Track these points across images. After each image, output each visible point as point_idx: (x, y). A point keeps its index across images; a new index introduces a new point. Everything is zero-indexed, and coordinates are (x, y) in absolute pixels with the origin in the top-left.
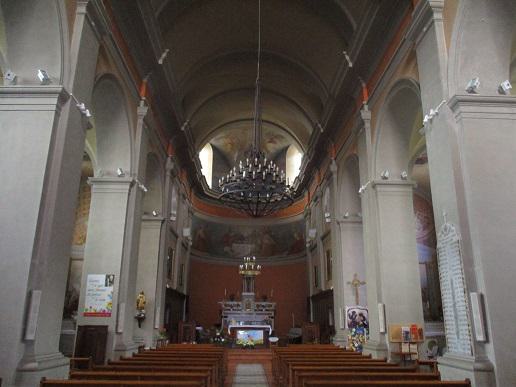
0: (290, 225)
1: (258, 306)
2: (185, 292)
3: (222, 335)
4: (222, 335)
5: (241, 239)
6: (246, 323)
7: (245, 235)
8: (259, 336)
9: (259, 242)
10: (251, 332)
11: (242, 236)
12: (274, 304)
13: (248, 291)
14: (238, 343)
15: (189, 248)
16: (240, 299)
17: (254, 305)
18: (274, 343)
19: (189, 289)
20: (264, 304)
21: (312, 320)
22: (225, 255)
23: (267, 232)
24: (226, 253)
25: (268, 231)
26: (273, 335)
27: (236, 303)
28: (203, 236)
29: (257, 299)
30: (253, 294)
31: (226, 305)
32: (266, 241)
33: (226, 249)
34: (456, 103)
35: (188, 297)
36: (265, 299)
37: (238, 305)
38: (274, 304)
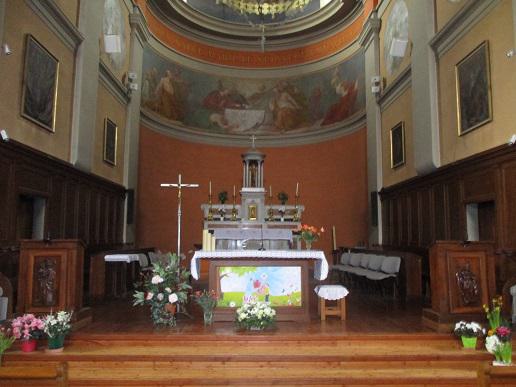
0: (327, 72)
1: (271, 212)
2: (126, 184)
3: (172, 282)
4: (172, 282)
5: (239, 101)
6: (250, 245)
7: (248, 94)
8: (287, 284)
9: (272, 107)
10: (263, 273)
11: (242, 97)
12: (300, 208)
13: (253, 185)
14: (221, 303)
15: (136, 97)
16: (238, 198)
17: (263, 210)
18: (331, 304)
19: (140, 170)
20: (282, 208)
21: (471, 238)
22: (214, 127)
23: (285, 89)
24: (215, 124)
25: (288, 87)
26: (330, 281)
27: (230, 207)
28: (169, 88)
29: (268, 200)
30: (263, 190)
31: (211, 211)
32: (283, 105)
33: (214, 117)
34: (381, 99)
35: (131, 192)
36: (283, 199)
37: (235, 211)
38: (300, 208)
